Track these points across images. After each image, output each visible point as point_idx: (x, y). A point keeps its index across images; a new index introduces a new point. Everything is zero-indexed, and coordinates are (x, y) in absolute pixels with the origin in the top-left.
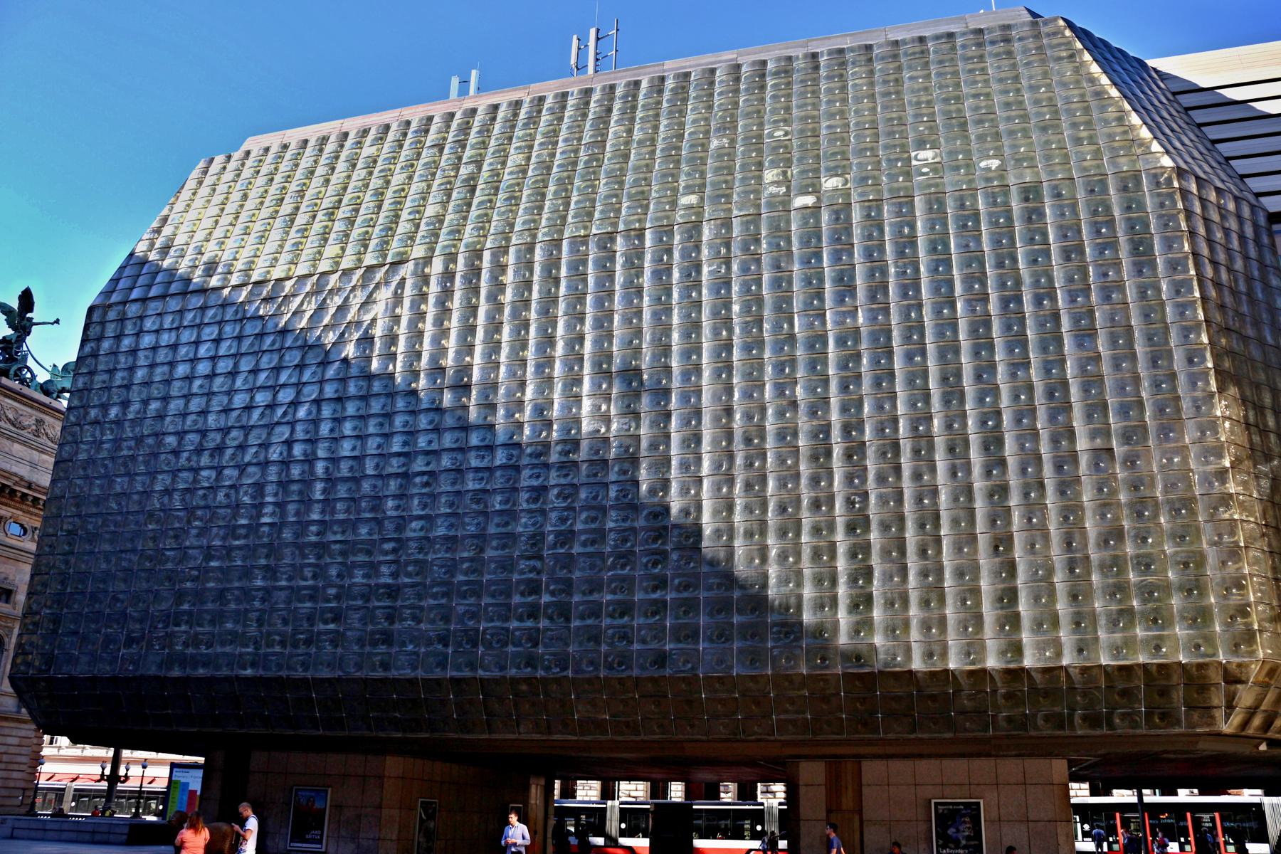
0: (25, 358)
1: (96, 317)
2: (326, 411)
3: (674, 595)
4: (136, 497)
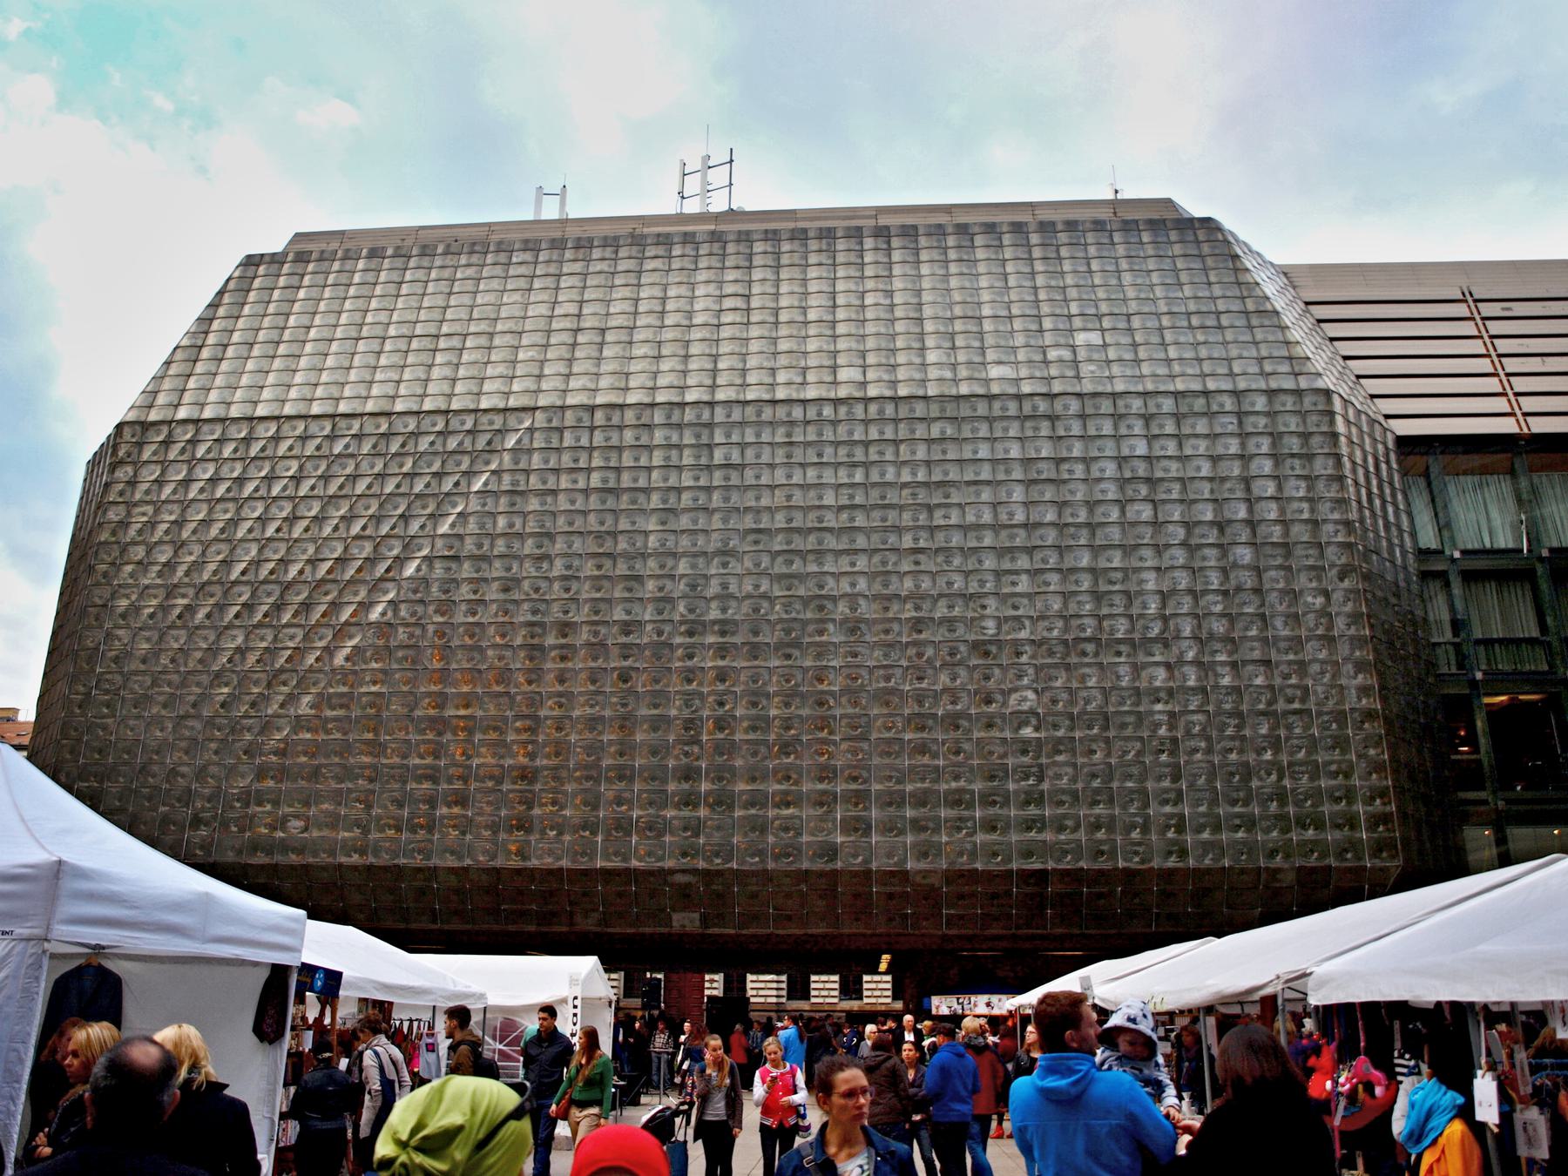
2: (439, 571)
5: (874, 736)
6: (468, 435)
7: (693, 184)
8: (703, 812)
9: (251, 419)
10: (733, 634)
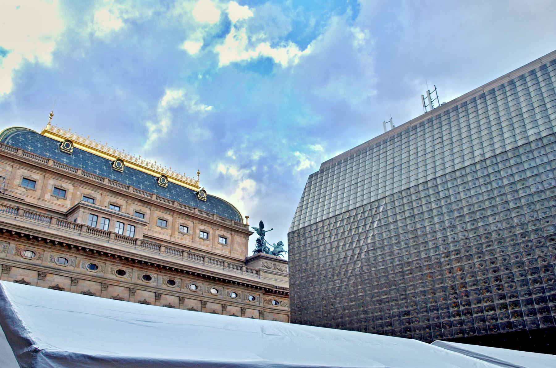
0: (265, 244)
1: (291, 237)
2: (371, 255)
3: (509, 300)
4: (317, 293)
5: (516, 279)
6: (369, 210)
7: (427, 101)
8: (463, 317)
9: (316, 223)
10: (493, 245)
